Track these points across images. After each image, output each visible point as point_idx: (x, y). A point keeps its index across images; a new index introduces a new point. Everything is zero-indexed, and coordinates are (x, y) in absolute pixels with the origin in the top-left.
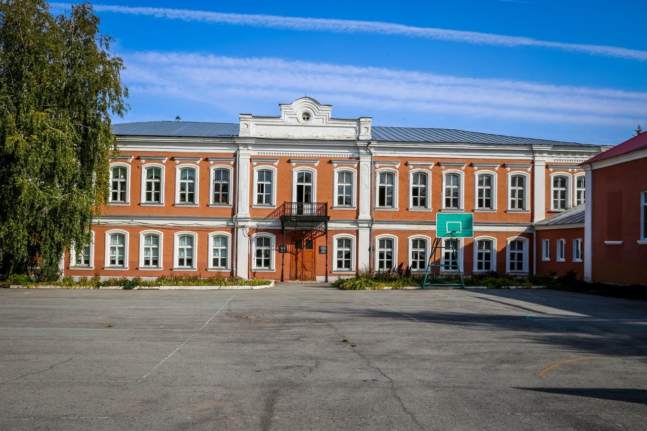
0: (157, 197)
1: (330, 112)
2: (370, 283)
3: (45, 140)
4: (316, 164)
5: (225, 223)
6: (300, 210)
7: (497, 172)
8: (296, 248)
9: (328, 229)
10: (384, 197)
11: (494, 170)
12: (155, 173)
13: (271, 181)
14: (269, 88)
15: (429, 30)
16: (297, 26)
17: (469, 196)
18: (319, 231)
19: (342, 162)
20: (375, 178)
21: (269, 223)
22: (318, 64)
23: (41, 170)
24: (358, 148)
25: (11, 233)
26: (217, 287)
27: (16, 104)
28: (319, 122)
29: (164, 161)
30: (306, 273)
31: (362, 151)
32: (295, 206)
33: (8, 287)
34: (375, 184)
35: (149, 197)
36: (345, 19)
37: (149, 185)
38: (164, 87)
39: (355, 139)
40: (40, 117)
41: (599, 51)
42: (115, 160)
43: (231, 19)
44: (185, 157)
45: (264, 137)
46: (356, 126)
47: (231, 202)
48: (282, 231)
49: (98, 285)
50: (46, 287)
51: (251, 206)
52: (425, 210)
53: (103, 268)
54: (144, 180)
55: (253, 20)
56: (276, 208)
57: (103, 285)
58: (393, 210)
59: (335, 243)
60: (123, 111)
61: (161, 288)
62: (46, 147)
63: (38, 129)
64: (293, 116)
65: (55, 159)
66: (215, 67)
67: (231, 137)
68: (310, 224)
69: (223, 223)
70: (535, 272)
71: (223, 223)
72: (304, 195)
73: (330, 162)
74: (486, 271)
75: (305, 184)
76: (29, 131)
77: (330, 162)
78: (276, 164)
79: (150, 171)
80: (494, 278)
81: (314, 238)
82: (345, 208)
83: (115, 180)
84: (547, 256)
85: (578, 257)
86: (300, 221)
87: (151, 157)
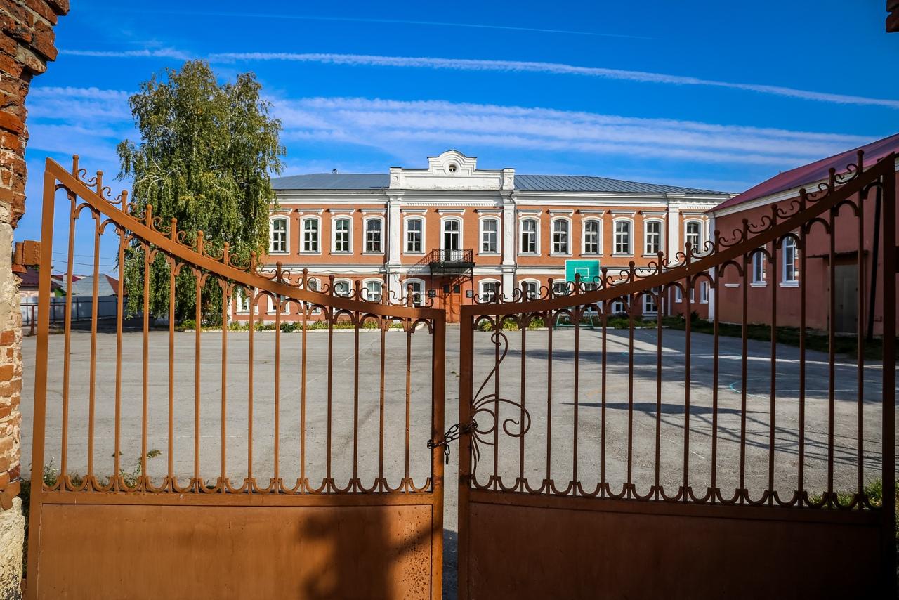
0: (315, 247)
1: (475, 164)
2: (507, 325)
3: (211, 198)
4: (463, 214)
5: (377, 270)
6: (448, 257)
7: (634, 219)
8: (445, 292)
10: (528, 244)
11: (631, 217)
12: (312, 224)
13: (420, 230)
14: (435, 130)
15: (595, 69)
16: (463, 68)
17: (608, 242)
18: (466, 276)
19: (486, 210)
20: (518, 225)
21: (419, 270)
22: (484, 104)
23: (209, 225)
24: (502, 197)
25: (184, 283)
26: (367, 330)
27: (188, 167)
28: (465, 174)
29: (321, 213)
30: (454, 316)
31: (505, 200)
32: (443, 253)
33: (183, 331)
34: (518, 231)
35: (307, 247)
36: (511, 60)
37: (307, 236)
38: (330, 131)
39: (499, 189)
40: (208, 178)
41: (765, 91)
42: (275, 213)
43: (397, 62)
44: (340, 209)
45: (413, 188)
46: (499, 176)
47: (383, 250)
48: (431, 277)
49: (261, 329)
50: (215, 331)
51: (401, 254)
52: (566, 256)
53: (266, 313)
54: (334, 231)
55: (419, 62)
56: (425, 255)
57: (265, 329)
58: (535, 255)
59: (481, 287)
60: (280, 169)
61: (317, 331)
62: (213, 204)
63: (206, 188)
64: (440, 168)
65: (221, 215)
66: (381, 111)
67: (381, 188)
68: (457, 270)
69: (376, 270)
70: (669, 314)
71: (376, 270)
72: (452, 242)
73: (476, 211)
74: (618, 312)
75: (452, 232)
76: (199, 191)
77: (476, 211)
78: (425, 213)
79: (307, 222)
80: (621, 319)
81: (461, 283)
82: (490, 254)
83: (276, 231)
84: (679, 298)
85: (705, 299)
86: (447, 268)
87: (308, 209)
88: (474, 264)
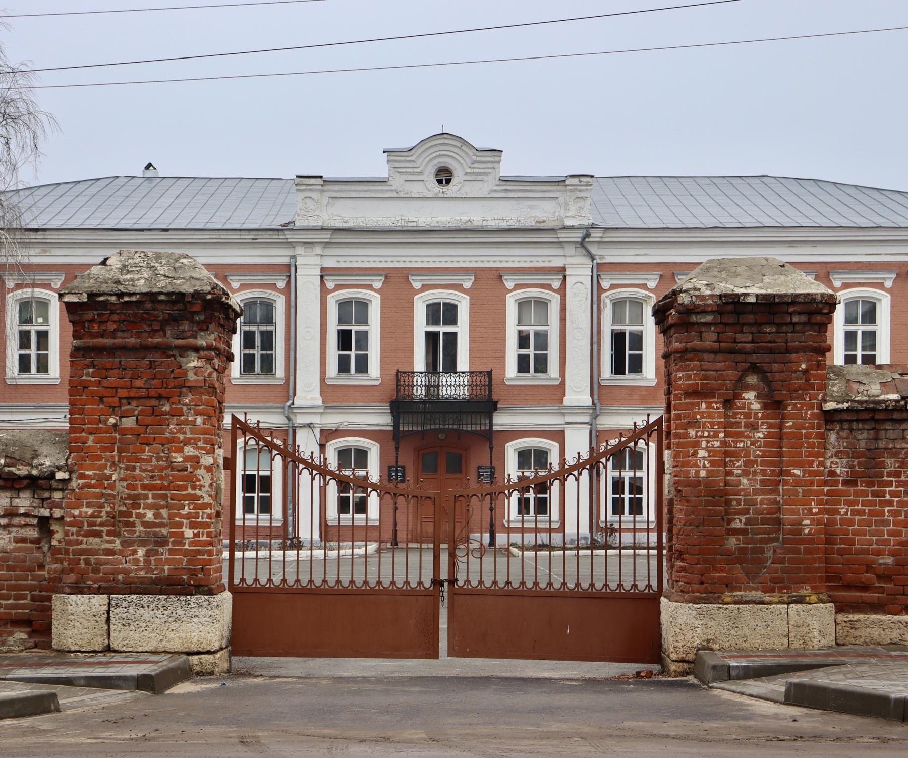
9: (495, 428)
72: (442, 350)
75: (442, 329)
83: (851, 328)
88: (496, 403)
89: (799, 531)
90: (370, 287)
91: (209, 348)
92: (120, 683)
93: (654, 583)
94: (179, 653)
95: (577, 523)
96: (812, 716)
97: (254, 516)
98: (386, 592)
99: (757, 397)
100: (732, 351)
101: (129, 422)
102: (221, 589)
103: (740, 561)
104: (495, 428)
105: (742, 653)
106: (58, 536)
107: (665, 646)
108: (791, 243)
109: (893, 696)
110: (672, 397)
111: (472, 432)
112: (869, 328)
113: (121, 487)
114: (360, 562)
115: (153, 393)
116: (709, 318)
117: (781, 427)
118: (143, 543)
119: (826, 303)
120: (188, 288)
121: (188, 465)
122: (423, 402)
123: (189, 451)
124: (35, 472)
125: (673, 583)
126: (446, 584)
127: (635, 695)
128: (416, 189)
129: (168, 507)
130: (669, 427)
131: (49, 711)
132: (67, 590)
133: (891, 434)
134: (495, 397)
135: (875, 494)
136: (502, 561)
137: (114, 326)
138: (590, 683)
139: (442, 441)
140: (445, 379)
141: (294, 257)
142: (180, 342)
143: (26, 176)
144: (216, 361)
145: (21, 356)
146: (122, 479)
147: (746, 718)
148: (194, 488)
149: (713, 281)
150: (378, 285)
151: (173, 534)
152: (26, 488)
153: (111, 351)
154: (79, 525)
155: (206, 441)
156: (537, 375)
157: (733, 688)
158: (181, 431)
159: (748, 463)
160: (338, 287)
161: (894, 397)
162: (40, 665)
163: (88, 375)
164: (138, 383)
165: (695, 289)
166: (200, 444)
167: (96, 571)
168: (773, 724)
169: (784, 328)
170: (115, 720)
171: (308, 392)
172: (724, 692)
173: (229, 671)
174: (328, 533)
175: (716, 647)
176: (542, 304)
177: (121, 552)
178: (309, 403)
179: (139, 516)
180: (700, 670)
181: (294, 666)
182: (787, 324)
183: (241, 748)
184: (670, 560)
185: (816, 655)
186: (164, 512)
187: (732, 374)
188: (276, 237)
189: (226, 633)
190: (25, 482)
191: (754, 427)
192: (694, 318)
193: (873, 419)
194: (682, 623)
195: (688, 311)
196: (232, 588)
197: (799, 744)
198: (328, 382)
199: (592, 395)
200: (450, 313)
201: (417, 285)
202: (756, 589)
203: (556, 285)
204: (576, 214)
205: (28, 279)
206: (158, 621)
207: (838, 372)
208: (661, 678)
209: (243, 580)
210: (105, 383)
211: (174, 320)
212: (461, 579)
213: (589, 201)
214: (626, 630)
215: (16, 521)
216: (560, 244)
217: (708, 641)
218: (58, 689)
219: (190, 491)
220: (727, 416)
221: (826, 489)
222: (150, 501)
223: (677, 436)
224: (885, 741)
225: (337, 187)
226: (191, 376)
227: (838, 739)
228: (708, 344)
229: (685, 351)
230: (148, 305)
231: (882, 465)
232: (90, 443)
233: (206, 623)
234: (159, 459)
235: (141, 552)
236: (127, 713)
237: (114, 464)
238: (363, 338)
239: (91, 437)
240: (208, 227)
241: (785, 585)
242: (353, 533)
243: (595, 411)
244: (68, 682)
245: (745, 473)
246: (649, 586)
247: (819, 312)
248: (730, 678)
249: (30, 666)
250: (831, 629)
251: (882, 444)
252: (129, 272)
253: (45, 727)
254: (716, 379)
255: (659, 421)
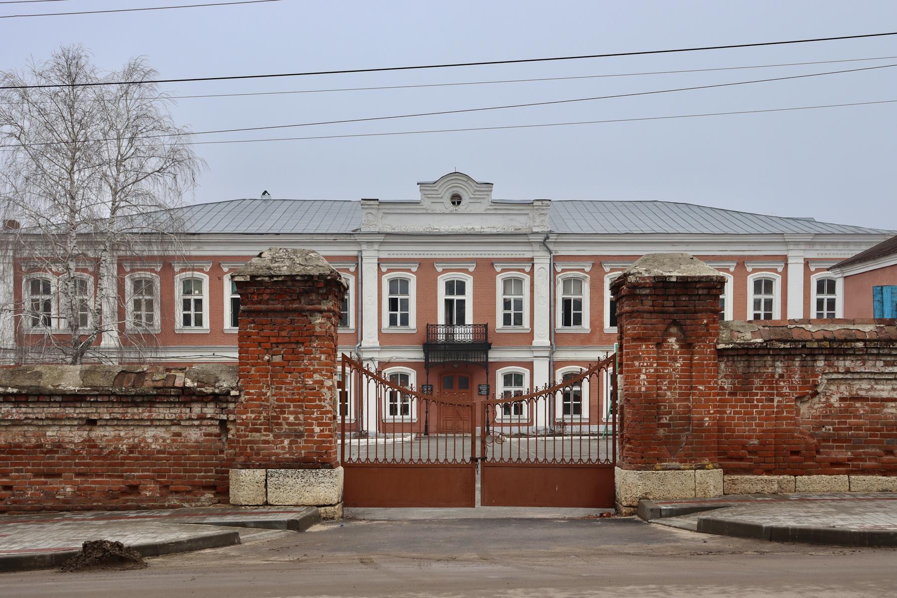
9: (490, 360)
54: (751, 297)
75: (456, 297)
83: (821, 297)
89: (702, 425)
90: (409, 271)
91: (329, 311)
92: (277, 525)
93: (610, 457)
94: (312, 506)
95: (542, 421)
96: (714, 539)
97: (569, 416)
98: (442, 466)
99: (677, 341)
100: (662, 312)
101: (277, 359)
102: (337, 465)
103: (665, 443)
104: (490, 360)
105: (667, 501)
106: (232, 432)
107: (619, 497)
108: (673, 244)
109: (764, 525)
110: (624, 341)
111: (475, 363)
112: (768, 297)
113: (273, 400)
114: (402, 446)
115: (293, 340)
116: (647, 291)
117: (691, 359)
118: (287, 436)
119: (719, 282)
120: (315, 272)
121: (316, 386)
122: (444, 344)
123: (317, 377)
124: (217, 391)
125: (623, 458)
126: (479, 461)
127: (604, 528)
128: (438, 208)
129: (303, 413)
130: (621, 360)
131: (233, 543)
132: (239, 466)
133: (758, 364)
134: (490, 341)
135: (747, 401)
136: (497, 446)
137: (268, 297)
138: (572, 521)
139: (456, 369)
140: (458, 330)
141: (361, 251)
142: (310, 307)
143: (188, 199)
144: (333, 319)
145: (505, 314)
146: (273, 395)
147: (675, 541)
148: (320, 400)
149: (649, 268)
150: (414, 269)
151: (307, 430)
152: (211, 401)
153: (266, 313)
154: (247, 425)
155: (327, 371)
156: (516, 326)
157: (664, 522)
158: (311, 364)
159: (671, 383)
160: (389, 271)
161: (760, 340)
162: (224, 514)
163: (251, 329)
164: (284, 333)
165: (638, 273)
166: (324, 372)
167: (258, 454)
168: (692, 544)
169: (694, 298)
170: (277, 549)
171: (370, 338)
172: (658, 525)
173: (342, 517)
174: (384, 427)
175: (651, 497)
176: (519, 281)
177: (273, 442)
178: (371, 345)
179: (285, 419)
180: (642, 512)
181: (380, 513)
182: (695, 295)
183: (361, 565)
184: (621, 443)
185: (713, 501)
186: (301, 416)
187: (661, 326)
188: (348, 239)
189: (341, 493)
190: (211, 397)
191: (675, 360)
192: (638, 291)
193: (747, 354)
194: (629, 483)
195: (634, 287)
196: (343, 464)
197: (711, 556)
198: (383, 332)
199: (550, 339)
200: (461, 288)
201: (439, 269)
202: (675, 461)
203: (528, 269)
204: (540, 224)
205: (190, 265)
206: (298, 486)
207: (727, 325)
208: (616, 517)
209: (350, 459)
210: (262, 334)
211: (307, 293)
212: (489, 457)
213: (547, 217)
214: (591, 487)
215: (205, 422)
216: (530, 243)
217: (646, 494)
218: (237, 529)
219: (317, 402)
220: (658, 353)
221: (718, 398)
222: (292, 409)
223: (627, 365)
224: (762, 553)
225: (388, 206)
226: (318, 329)
227: (733, 553)
228: (646, 308)
229: (632, 312)
230: (290, 283)
231: (752, 383)
232: (253, 372)
233: (327, 487)
234: (297, 382)
235: (286, 442)
236: (284, 545)
237: (268, 386)
238: (405, 303)
239: (253, 369)
240: (305, 232)
241: (693, 458)
242: (403, 428)
243: (552, 349)
244: (243, 525)
245: (669, 389)
246: (607, 460)
247: (715, 288)
248: (661, 516)
249: (218, 515)
250: (721, 485)
251: (752, 370)
252: (276, 262)
253: (233, 554)
254: (651, 330)
255: (614, 356)
